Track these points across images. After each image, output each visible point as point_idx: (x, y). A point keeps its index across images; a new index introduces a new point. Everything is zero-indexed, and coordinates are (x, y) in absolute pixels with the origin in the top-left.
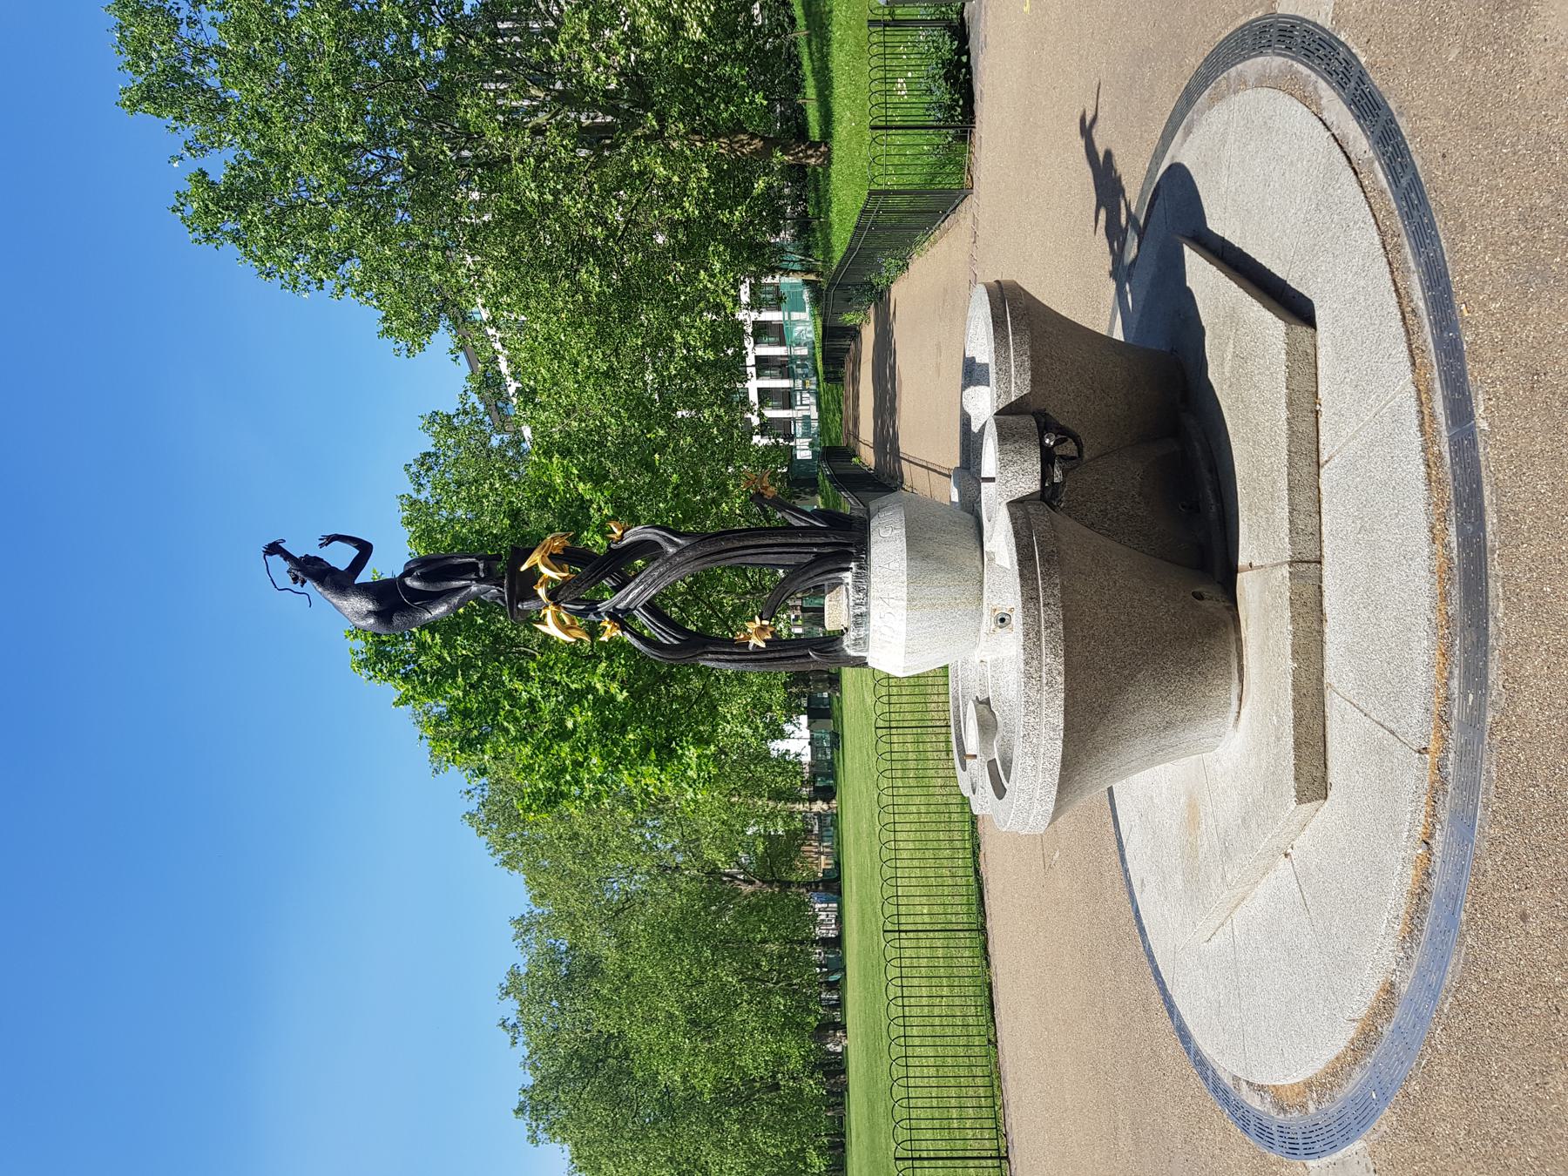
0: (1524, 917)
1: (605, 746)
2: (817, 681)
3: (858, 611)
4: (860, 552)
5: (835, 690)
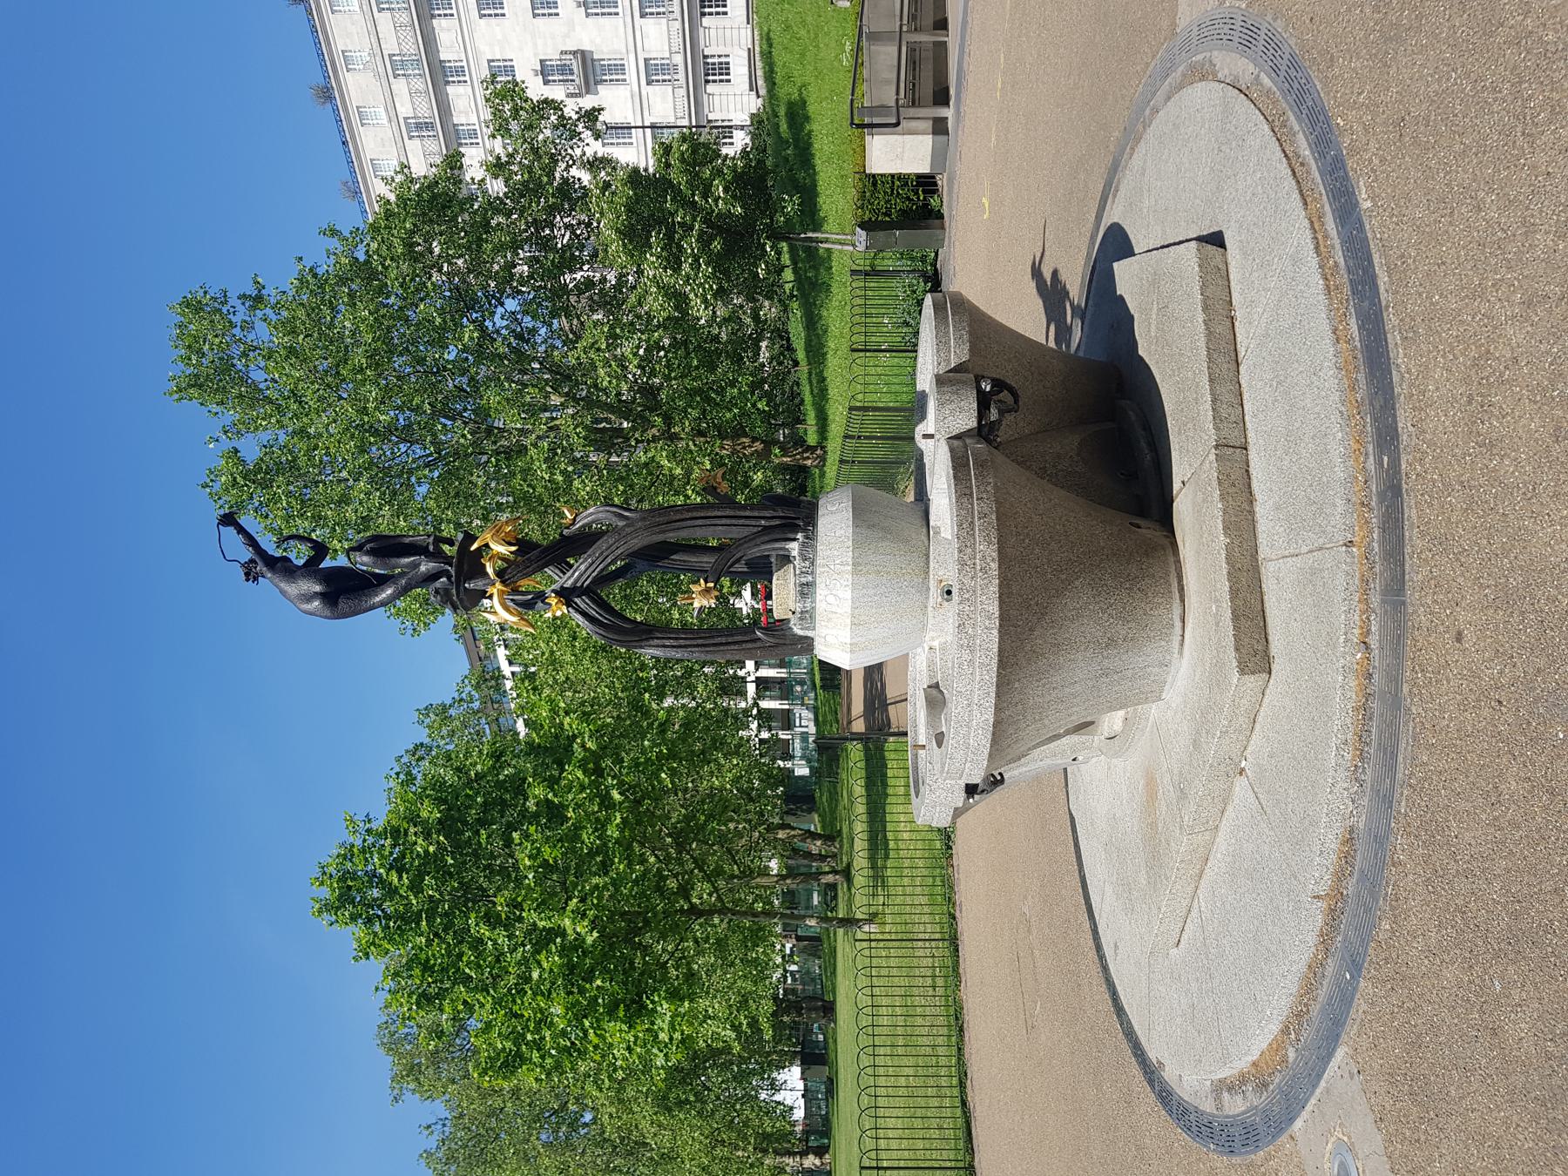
0: (1459, 637)
1: (569, 993)
2: (809, 1010)
3: (804, 580)
4: (808, 524)
5: (830, 1020)
